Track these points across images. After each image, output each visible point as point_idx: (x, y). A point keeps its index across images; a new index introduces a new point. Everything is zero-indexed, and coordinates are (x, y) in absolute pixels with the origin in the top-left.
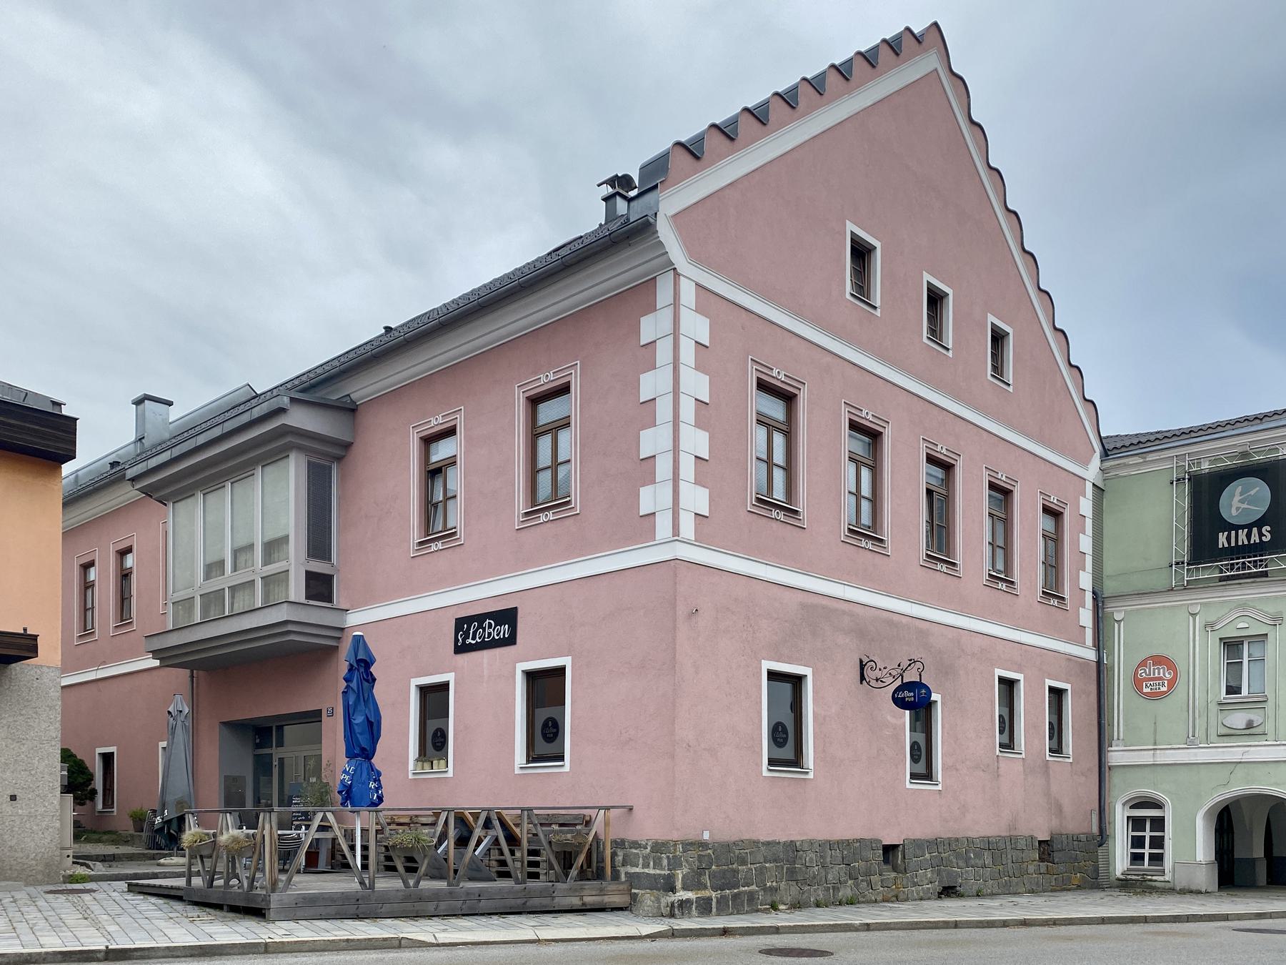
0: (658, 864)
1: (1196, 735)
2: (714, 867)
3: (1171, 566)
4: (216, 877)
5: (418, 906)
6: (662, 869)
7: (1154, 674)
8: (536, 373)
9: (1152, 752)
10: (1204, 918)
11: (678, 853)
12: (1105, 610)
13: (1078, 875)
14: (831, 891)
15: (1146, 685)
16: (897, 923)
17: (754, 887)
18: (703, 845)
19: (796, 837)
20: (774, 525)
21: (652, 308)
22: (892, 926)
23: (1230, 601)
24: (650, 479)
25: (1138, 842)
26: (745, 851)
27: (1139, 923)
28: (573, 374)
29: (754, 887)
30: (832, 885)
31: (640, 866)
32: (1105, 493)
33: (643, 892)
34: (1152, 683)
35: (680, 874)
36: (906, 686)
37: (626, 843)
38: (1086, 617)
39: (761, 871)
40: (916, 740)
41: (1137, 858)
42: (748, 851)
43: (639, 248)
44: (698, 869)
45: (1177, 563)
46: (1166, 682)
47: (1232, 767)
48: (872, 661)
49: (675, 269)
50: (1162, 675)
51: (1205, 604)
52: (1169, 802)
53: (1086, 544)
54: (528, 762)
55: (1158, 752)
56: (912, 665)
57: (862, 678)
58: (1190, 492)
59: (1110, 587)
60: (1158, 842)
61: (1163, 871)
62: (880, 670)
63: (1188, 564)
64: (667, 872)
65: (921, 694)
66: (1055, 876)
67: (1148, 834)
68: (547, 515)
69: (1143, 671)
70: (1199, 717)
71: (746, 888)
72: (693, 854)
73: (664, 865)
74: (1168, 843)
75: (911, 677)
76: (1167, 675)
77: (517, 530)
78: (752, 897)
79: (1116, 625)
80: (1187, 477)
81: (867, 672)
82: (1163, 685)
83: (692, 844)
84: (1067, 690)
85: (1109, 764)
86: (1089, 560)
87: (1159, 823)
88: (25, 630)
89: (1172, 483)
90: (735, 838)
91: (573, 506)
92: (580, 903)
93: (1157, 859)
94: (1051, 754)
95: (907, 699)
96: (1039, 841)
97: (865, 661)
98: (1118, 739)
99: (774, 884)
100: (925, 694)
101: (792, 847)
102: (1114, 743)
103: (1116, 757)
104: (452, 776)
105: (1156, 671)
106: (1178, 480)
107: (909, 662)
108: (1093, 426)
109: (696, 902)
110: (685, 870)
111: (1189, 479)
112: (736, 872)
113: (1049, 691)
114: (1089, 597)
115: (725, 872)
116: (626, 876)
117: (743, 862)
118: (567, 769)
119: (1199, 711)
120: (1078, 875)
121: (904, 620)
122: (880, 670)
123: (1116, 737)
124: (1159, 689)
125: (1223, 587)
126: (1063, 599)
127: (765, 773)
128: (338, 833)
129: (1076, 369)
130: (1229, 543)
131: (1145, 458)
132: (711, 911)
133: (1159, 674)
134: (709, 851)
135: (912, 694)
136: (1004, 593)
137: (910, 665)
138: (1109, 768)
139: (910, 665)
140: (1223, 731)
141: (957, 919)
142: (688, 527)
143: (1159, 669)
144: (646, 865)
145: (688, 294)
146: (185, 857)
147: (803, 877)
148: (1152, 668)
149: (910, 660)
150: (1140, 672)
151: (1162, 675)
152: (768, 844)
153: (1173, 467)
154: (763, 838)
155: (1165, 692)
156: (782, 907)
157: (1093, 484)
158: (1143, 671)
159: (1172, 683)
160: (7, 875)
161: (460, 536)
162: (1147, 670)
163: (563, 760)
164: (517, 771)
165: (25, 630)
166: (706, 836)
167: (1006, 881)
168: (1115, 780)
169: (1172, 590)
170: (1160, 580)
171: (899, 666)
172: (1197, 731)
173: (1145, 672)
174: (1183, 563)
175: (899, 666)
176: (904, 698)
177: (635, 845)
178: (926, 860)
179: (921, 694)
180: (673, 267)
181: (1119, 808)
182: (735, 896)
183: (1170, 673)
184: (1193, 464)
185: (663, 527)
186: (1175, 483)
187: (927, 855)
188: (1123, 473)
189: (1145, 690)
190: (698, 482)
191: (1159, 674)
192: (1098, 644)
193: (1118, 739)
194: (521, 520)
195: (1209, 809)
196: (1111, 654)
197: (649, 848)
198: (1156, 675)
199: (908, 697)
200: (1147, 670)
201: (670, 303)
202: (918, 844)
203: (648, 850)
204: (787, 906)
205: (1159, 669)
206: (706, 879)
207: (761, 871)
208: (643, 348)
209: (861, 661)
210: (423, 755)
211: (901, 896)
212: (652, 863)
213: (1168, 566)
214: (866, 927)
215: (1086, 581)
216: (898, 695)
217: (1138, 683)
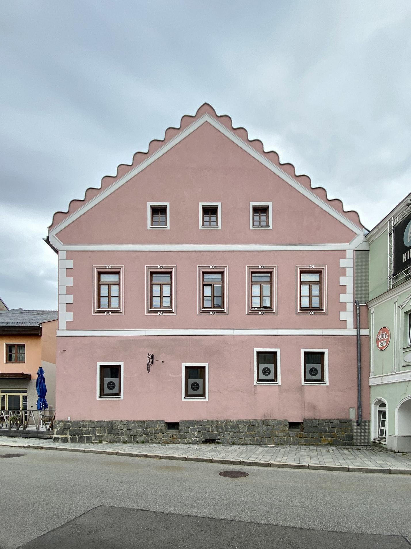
1: (395, 368)
2: (71, 428)
4: (21, 426)
5: (17, 434)
9: (381, 378)
10: (252, 464)
11: (56, 424)
12: (369, 309)
14: (133, 438)
16: (94, 451)
17: (90, 435)
18: (67, 422)
19: (113, 419)
20: (107, 317)
22: (92, 452)
23: (408, 291)
34: (382, 342)
39: (93, 431)
42: (88, 424)
47: (407, 383)
50: (385, 337)
51: (398, 296)
55: (383, 377)
70: (396, 357)
71: (86, 435)
72: (62, 425)
74: (386, 424)
76: (386, 337)
79: (371, 315)
83: (61, 421)
85: (369, 385)
88: (22, 373)
90: (82, 420)
92: (50, 436)
101: (111, 422)
109: (61, 438)
119: (396, 354)
121: (183, 337)
123: (371, 372)
125: (404, 284)
127: (98, 398)
128: (4, 416)
130: (407, 258)
131: (379, 227)
132: (68, 441)
134: (69, 423)
140: (405, 364)
152: (98, 421)
162: (381, 336)
165: (22, 373)
166: (69, 419)
172: (395, 366)
181: (373, 407)
182: (80, 438)
188: (374, 239)
195: (400, 407)
200: (381, 336)
202: (191, 423)
211: (175, 442)
214: (84, 451)
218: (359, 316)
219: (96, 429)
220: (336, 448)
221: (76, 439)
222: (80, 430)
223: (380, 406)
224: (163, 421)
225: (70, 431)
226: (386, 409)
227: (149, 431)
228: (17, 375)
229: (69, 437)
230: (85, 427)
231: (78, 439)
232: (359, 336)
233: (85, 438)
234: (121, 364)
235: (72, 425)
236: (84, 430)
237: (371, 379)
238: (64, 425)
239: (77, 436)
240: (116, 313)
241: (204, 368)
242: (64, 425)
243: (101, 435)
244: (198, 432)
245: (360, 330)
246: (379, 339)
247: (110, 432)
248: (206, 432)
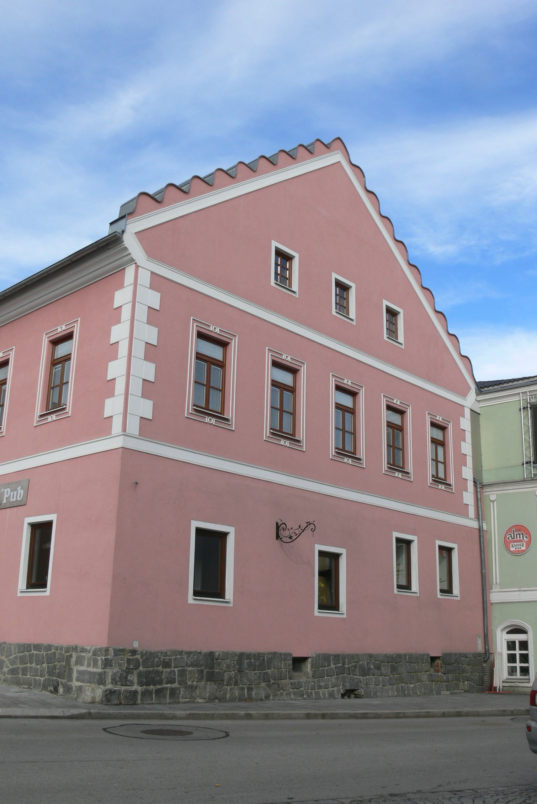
0: (95, 665)
3: (523, 464)
6: (97, 668)
7: (517, 538)
8: (56, 326)
13: (466, 682)
14: (246, 690)
15: (512, 546)
17: (176, 685)
18: (134, 652)
21: (121, 286)
24: (111, 393)
25: (511, 658)
27: (420, 718)
28: (76, 327)
29: (176, 685)
30: (248, 685)
31: (86, 665)
32: (480, 415)
33: (86, 685)
34: (516, 544)
35: (110, 672)
37: (78, 649)
38: (469, 498)
39: (182, 673)
41: (512, 671)
44: (127, 669)
45: (527, 463)
46: (524, 543)
48: (284, 524)
49: (136, 263)
52: (530, 627)
53: (467, 448)
54: (27, 588)
56: (309, 526)
57: (278, 537)
58: (531, 416)
59: (487, 478)
60: (525, 658)
61: (529, 679)
62: (288, 530)
63: (533, 463)
64: (100, 670)
66: (446, 683)
67: (518, 652)
68: (52, 417)
69: (510, 536)
73: (99, 665)
74: (531, 659)
77: (35, 426)
78: (173, 693)
79: (492, 504)
80: (529, 406)
81: (281, 532)
82: (523, 545)
84: (454, 548)
85: (491, 602)
86: (469, 460)
87: (524, 645)
89: (520, 410)
91: (67, 411)
93: (525, 671)
94: (441, 594)
96: (431, 657)
97: (280, 523)
98: (496, 584)
99: (195, 683)
102: (493, 587)
103: (495, 597)
104: (232, 606)
105: (518, 535)
106: (524, 408)
107: (306, 525)
108: (469, 373)
110: (116, 670)
111: (530, 408)
112: (160, 673)
113: (439, 549)
114: (470, 485)
115: (149, 672)
116: (77, 673)
120: (466, 682)
122: (288, 530)
123: (494, 582)
124: (520, 548)
126: (450, 485)
133: (520, 538)
136: (400, 479)
137: (307, 526)
138: (491, 604)
139: (307, 526)
141: (324, 712)
142: (134, 426)
143: (519, 534)
144: (89, 665)
145: (145, 278)
148: (515, 534)
149: (307, 523)
150: (508, 536)
151: (521, 538)
153: (520, 400)
155: (523, 551)
157: (471, 410)
158: (510, 536)
159: (528, 544)
160: (80, 678)
161: (3, 430)
162: (512, 535)
164: (19, 594)
166: (136, 645)
167: (402, 686)
168: (495, 614)
169: (524, 481)
170: (518, 474)
171: (300, 527)
173: (511, 536)
174: (530, 462)
175: (300, 527)
177: (83, 650)
178: (332, 669)
180: (135, 262)
182: (158, 692)
183: (526, 537)
184: (532, 398)
185: (117, 426)
186: (522, 410)
187: (333, 666)
189: (512, 549)
190: (144, 396)
191: (520, 538)
192: (479, 516)
193: (496, 584)
194: (38, 420)
196: (489, 524)
197: (92, 652)
198: (518, 538)
200: (512, 535)
201: (131, 283)
203: (91, 654)
204: (206, 700)
205: (519, 534)
206: (134, 678)
207: (182, 673)
208: (115, 310)
209: (277, 524)
210: (31, 585)
212: (92, 664)
213: (521, 464)
215: (468, 473)
217: (507, 545)
218: (481, 502)
219: (187, 670)
220: (98, 699)
221: (150, 693)
222: (157, 672)
223: (508, 633)
224: (290, 654)
225: (140, 675)
226: (529, 638)
227: (272, 676)
228: (410, 576)
229: (139, 689)
230: (167, 665)
231: (154, 695)
232: (480, 530)
233: (167, 690)
234: (231, 530)
235: (143, 661)
236: (166, 672)
237: (495, 593)
238: (128, 660)
239: (152, 687)
240: (295, 446)
241: (223, 536)
242: (128, 660)
243: (195, 683)
244: (336, 676)
245: (482, 522)
246: (509, 539)
247: (212, 677)
248: (345, 675)
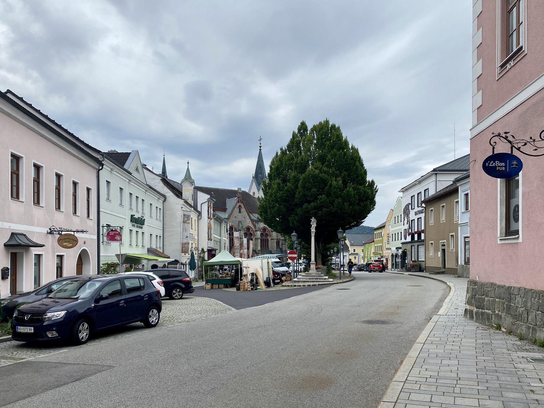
14: (531, 330)
26: (488, 289)
36: (495, 157)
40: (8, 89)
43: (60, 351)
54: (506, 235)
65: (513, 165)
75: (503, 148)
95: (498, 168)
100: (516, 165)
117: (487, 296)
118: (520, 240)
129: (23, 236)
135: (503, 164)
146: (356, 257)
147: (514, 313)
154: (498, 283)
156: (503, 329)
163: (518, 234)
176: (496, 167)
179: (513, 165)
199: (499, 166)
216: (489, 164)
